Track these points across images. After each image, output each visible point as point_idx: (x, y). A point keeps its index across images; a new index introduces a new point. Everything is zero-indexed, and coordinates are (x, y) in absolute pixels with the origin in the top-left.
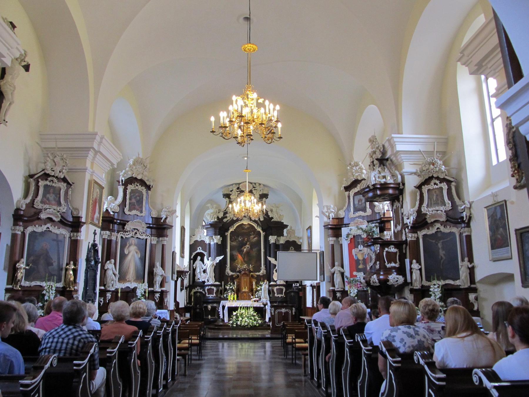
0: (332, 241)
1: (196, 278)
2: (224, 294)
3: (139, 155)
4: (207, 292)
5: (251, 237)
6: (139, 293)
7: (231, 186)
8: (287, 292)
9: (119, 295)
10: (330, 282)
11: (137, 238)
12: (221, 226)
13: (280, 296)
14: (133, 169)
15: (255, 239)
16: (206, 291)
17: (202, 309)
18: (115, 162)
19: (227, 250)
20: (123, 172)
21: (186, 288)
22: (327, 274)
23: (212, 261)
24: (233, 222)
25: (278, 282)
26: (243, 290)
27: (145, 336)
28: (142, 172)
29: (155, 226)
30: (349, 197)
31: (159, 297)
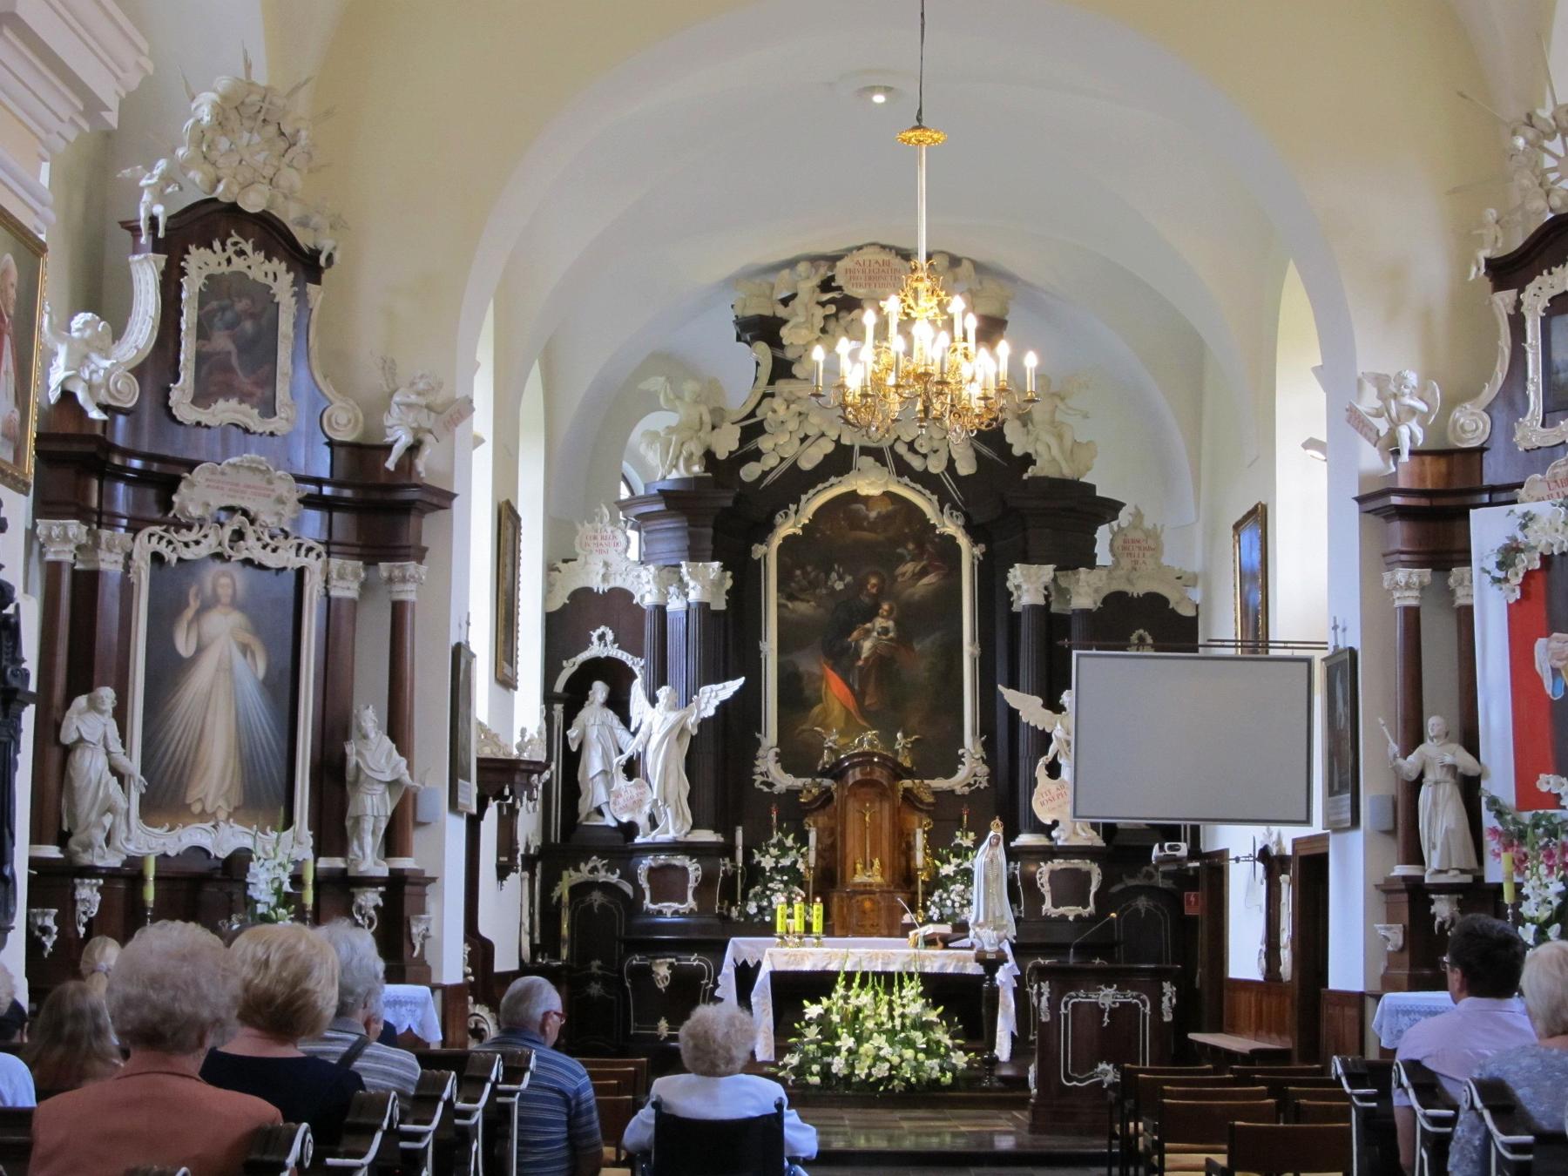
0: (1408, 586)
1: (584, 806)
2: (745, 898)
3: (248, 67)
4: (645, 885)
5: (901, 569)
6: (263, 883)
7: (786, 273)
8: (1115, 889)
9: (150, 894)
10: (1392, 833)
11: (248, 562)
12: (729, 503)
13: (1071, 912)
14: (214, 155)
15: (925, 580)
16: (643, 882)
17: (623, 982)
18: (108, 93)
19: (762, 645)
20: (157, 172)
21: (529, 862)
22: (1374, 789)
23: (673, 707)
24: (796, 482)
25: (1061, 837)
26: (859, 879)
27: (330, 1161)
28: (269, 172)
29: (347, 493)
30: (1517, 323)
31: (376, 908)
